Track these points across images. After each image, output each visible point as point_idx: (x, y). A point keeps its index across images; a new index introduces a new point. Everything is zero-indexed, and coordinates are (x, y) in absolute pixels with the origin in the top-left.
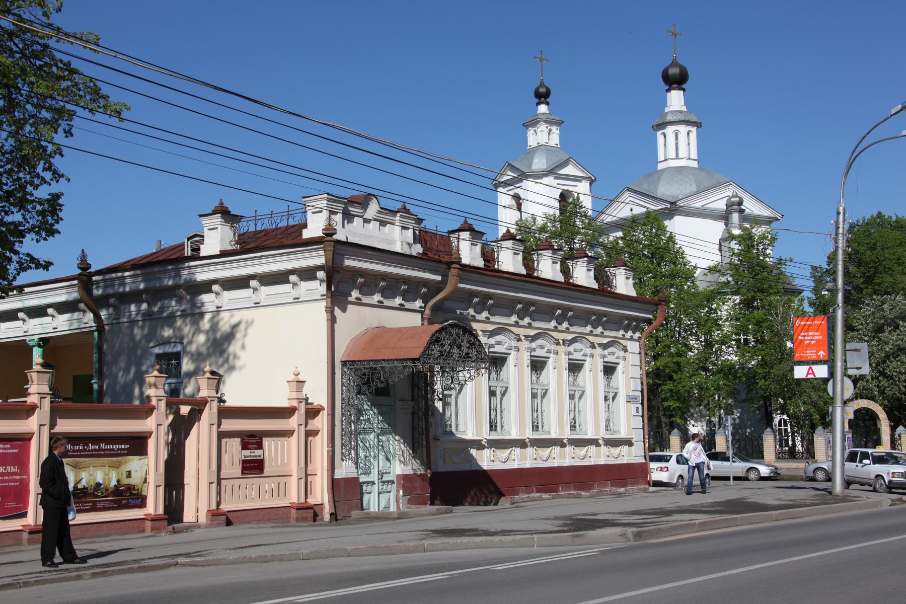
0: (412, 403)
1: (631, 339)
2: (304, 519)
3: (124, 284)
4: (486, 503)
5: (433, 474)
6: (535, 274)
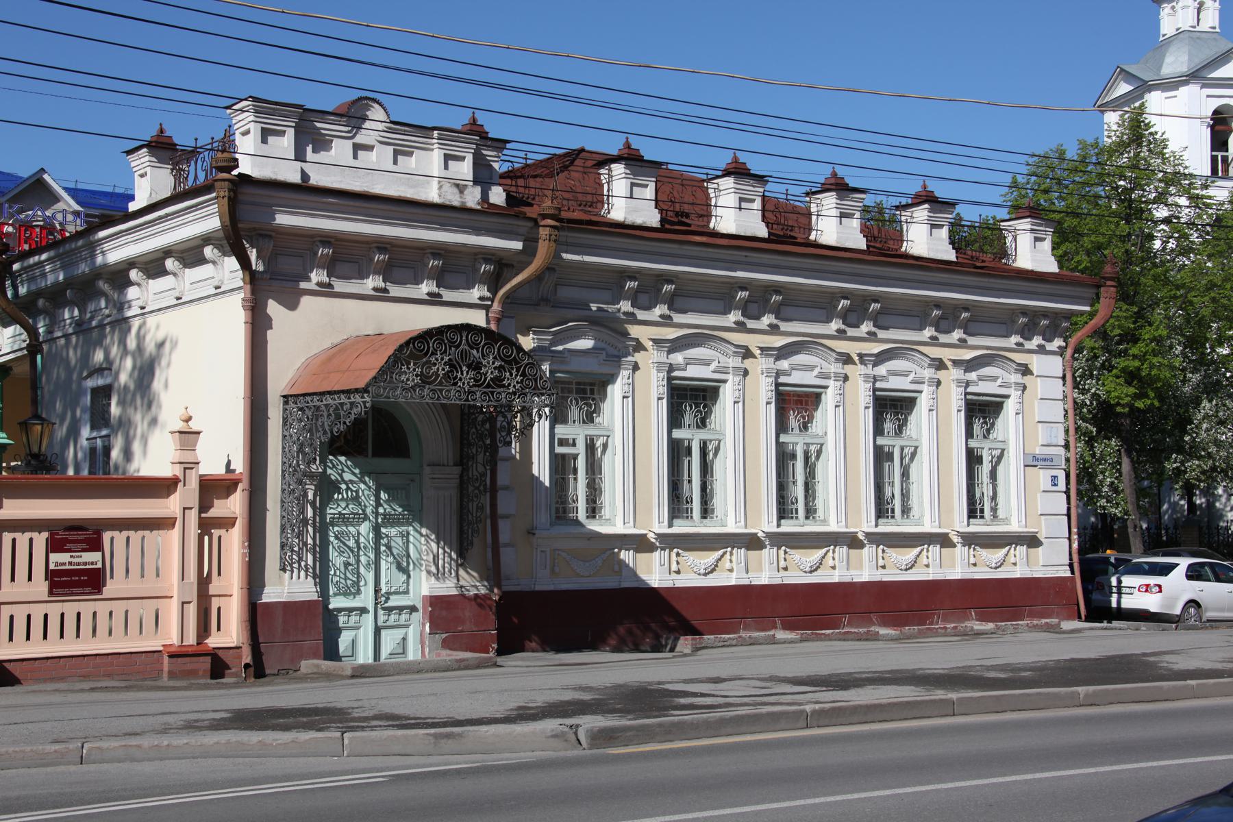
0: (457, 470)
1: (1041, 350)
2: (192, 673)
3: (44, 275)
4: (657, 648)
5: (505, 596)
6: (812, 237)
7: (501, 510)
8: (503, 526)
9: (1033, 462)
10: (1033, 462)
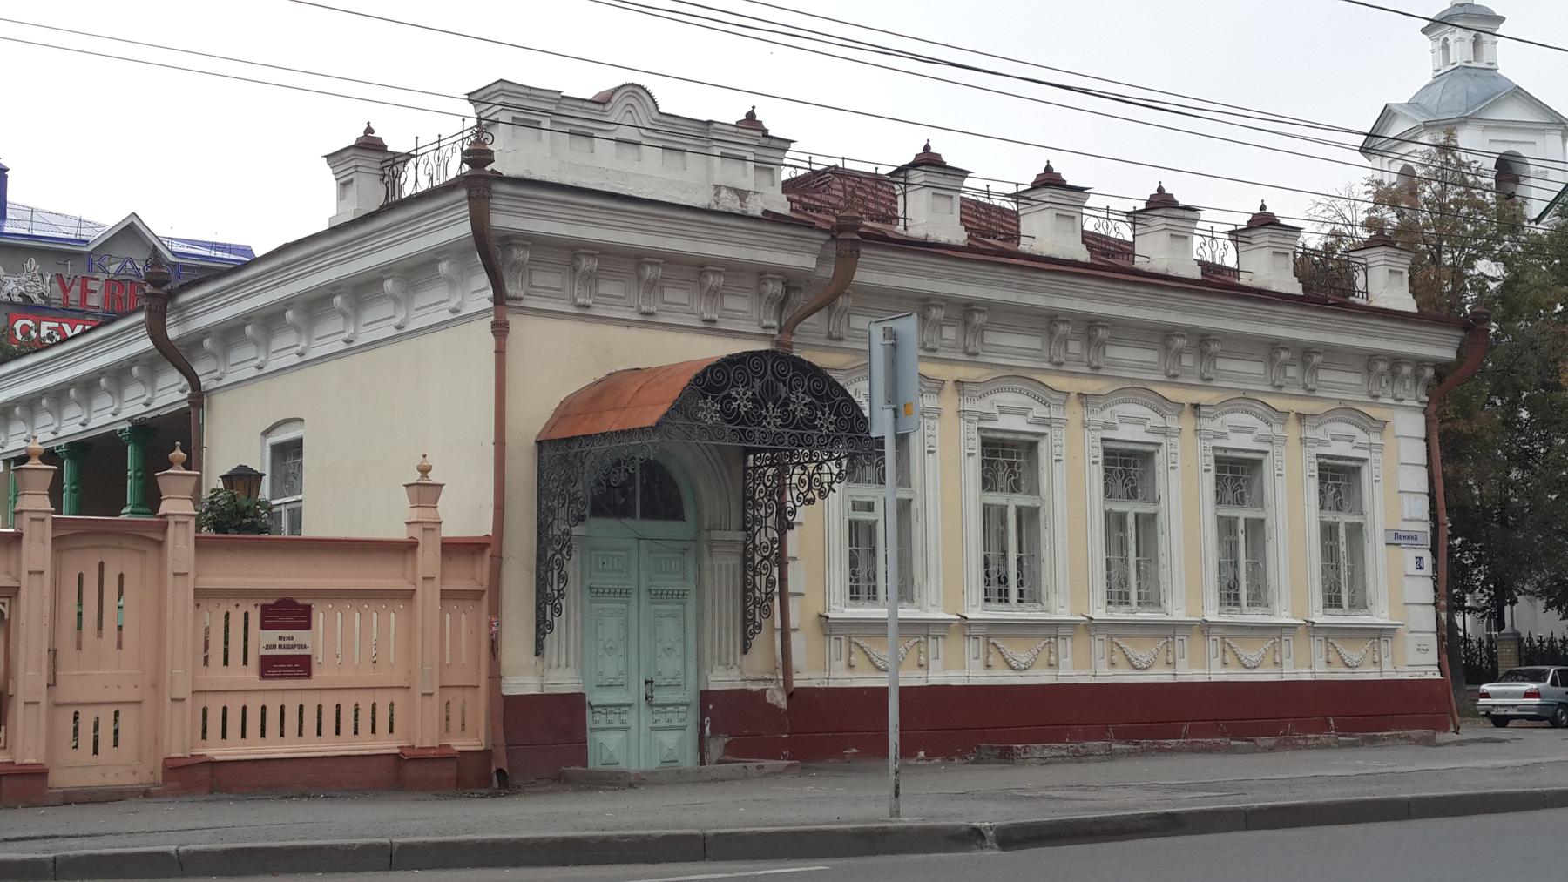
7: (792, 587)
8: (793, 604)
9: (1398, 539)
10: (1398, 539)
